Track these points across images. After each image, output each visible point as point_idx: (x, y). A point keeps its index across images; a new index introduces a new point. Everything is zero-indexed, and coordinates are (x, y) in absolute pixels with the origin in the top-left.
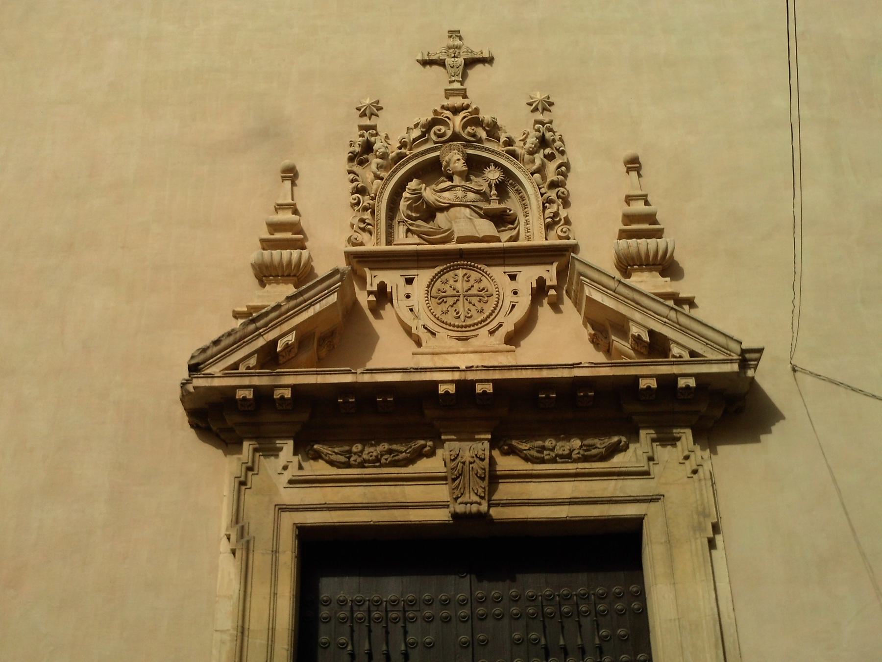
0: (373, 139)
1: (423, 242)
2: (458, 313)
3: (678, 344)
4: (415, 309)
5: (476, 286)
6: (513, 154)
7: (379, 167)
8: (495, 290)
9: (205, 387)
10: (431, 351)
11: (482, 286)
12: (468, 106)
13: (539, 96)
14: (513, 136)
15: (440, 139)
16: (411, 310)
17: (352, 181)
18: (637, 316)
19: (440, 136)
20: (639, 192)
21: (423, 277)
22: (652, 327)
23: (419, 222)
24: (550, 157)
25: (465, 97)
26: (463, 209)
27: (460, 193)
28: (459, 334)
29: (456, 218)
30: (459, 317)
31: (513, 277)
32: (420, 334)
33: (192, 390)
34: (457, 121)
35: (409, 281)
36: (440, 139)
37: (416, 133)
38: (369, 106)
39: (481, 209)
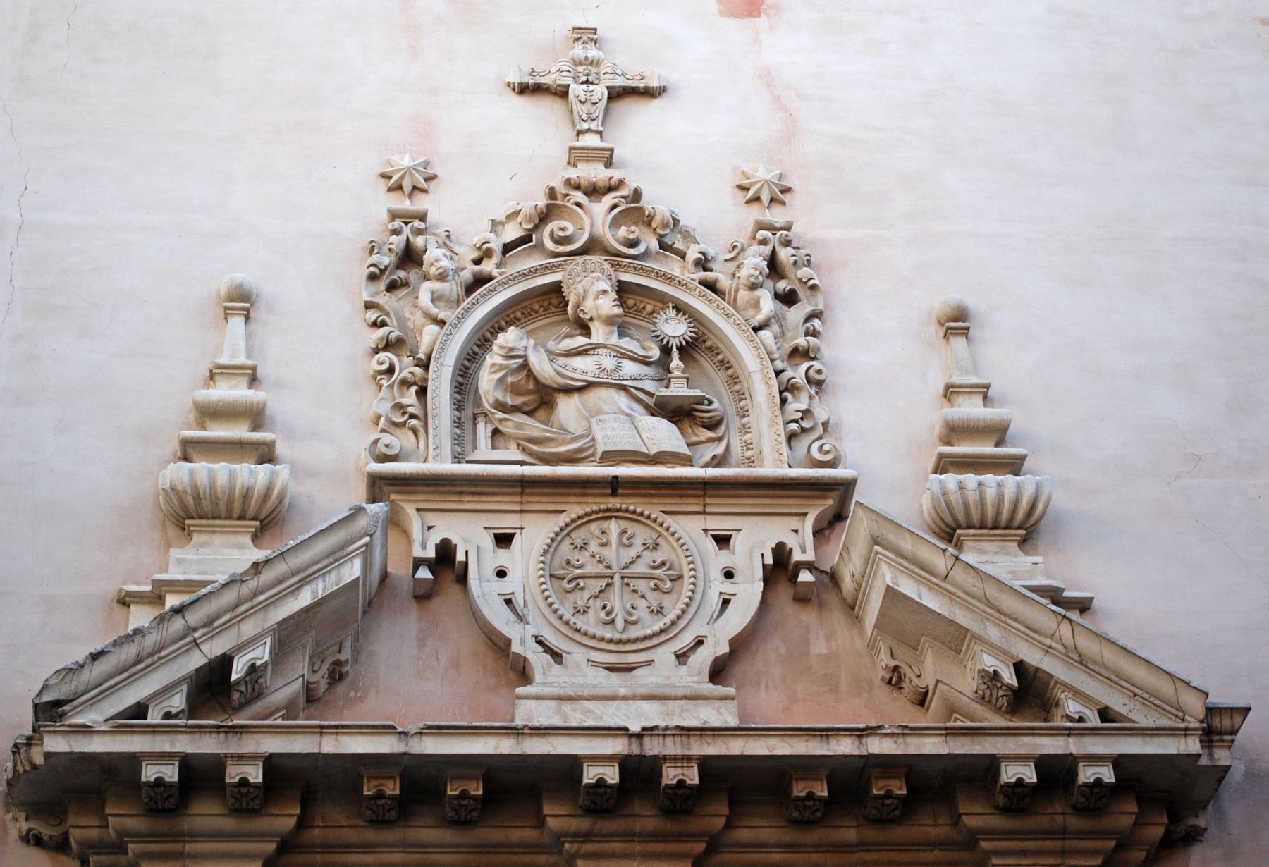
0: (419, 241)
1: (526, 459)
2: (608, 614)
4: (519, 601)
5: (648, 557)
6: (712, 286)
7: (436, 298)
8: (684, 562)
9: (71, 754)
11: (659, 557)
12: (621, 184)
13: (763, 173)
14: (711, 252)
15: (561, 249)
16: (509, 602)
18: (993, 633)
19: (559, 241)
20: (975, 380)
21: (535, 532)
22: (1022, 656)
23: (520, 418)
24: (788, 299)
26: (612, 393)
27: (609, 362)
28: (612, 659)
29: (600, 412)
30: (613, 621)
31: (723, 541)
32: (530, 656)
33: (39, 760)
34: (600, 209)
35: (504, 540)
36: (561, 249)
37: (512, 232)
38: (408, 171)
39: (651, 395)
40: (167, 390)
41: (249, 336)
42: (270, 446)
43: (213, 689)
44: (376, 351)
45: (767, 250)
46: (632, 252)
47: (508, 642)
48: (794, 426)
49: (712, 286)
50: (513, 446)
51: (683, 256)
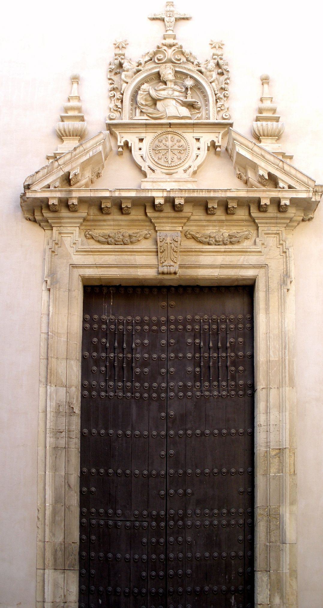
0: (122, 61)
1: (148, 118)
3: (283, 181)
4: (144, 157)
6: (201, 72)
7: (126, 76)
10: (151, 180)
11: (181, 144)
12: (177, 44)
14: (200, 62)
16: (142, 157)
17: (111, 84)
19: (159, 60)
21: (149, 137)
24: (222, 74)
25: (174, 38)
27: (170, 92)
31: (198, 140)
34: (170, 53)
35: (141, 140)
36: (160, 62)
37: (147, 58)
38: (120, 43)
40: (58, 102)
41: (78, 88)
42: (83, 117)
43: (67, 180)
44: (111, 91)
45: (216, 61)
46: (178, 62)
47: (141, 167)
48: (219, 109)
49: (201, 72)
50: (145, 115)
51: (193, 63)
